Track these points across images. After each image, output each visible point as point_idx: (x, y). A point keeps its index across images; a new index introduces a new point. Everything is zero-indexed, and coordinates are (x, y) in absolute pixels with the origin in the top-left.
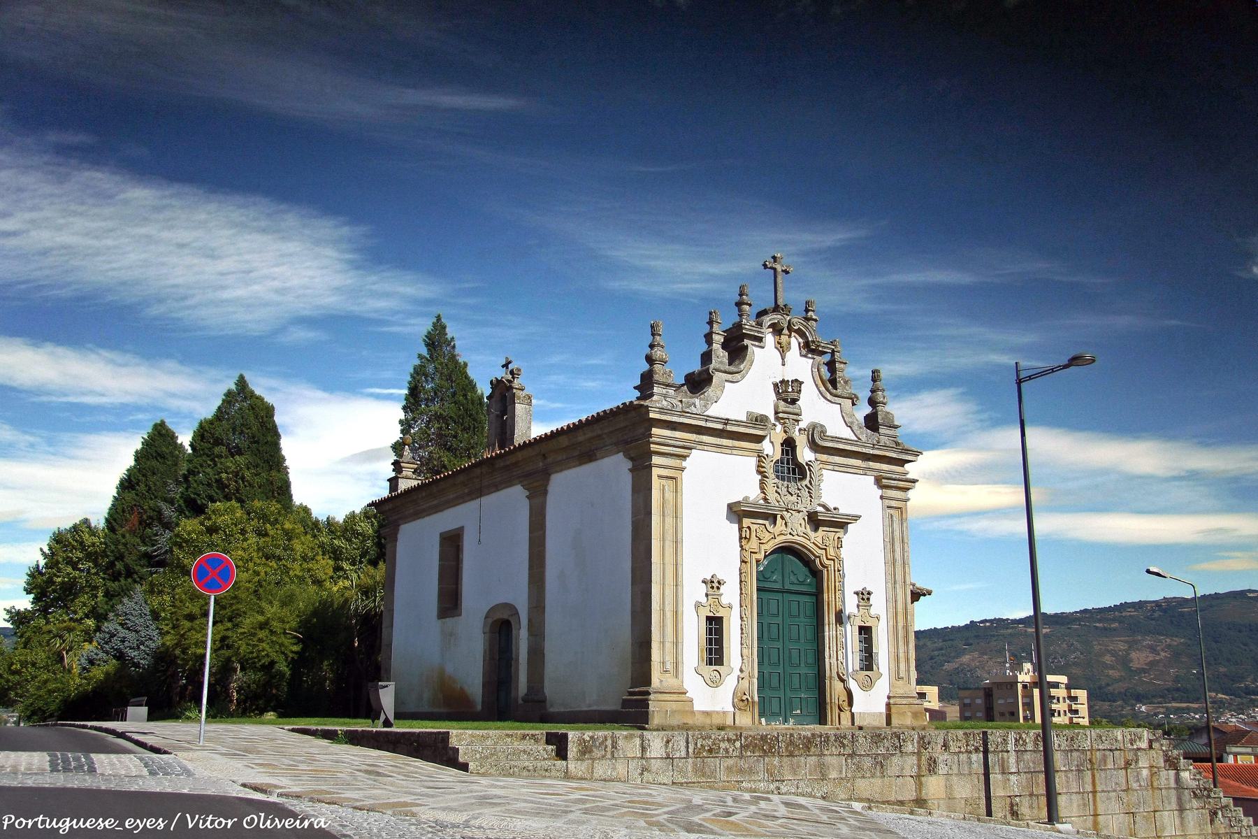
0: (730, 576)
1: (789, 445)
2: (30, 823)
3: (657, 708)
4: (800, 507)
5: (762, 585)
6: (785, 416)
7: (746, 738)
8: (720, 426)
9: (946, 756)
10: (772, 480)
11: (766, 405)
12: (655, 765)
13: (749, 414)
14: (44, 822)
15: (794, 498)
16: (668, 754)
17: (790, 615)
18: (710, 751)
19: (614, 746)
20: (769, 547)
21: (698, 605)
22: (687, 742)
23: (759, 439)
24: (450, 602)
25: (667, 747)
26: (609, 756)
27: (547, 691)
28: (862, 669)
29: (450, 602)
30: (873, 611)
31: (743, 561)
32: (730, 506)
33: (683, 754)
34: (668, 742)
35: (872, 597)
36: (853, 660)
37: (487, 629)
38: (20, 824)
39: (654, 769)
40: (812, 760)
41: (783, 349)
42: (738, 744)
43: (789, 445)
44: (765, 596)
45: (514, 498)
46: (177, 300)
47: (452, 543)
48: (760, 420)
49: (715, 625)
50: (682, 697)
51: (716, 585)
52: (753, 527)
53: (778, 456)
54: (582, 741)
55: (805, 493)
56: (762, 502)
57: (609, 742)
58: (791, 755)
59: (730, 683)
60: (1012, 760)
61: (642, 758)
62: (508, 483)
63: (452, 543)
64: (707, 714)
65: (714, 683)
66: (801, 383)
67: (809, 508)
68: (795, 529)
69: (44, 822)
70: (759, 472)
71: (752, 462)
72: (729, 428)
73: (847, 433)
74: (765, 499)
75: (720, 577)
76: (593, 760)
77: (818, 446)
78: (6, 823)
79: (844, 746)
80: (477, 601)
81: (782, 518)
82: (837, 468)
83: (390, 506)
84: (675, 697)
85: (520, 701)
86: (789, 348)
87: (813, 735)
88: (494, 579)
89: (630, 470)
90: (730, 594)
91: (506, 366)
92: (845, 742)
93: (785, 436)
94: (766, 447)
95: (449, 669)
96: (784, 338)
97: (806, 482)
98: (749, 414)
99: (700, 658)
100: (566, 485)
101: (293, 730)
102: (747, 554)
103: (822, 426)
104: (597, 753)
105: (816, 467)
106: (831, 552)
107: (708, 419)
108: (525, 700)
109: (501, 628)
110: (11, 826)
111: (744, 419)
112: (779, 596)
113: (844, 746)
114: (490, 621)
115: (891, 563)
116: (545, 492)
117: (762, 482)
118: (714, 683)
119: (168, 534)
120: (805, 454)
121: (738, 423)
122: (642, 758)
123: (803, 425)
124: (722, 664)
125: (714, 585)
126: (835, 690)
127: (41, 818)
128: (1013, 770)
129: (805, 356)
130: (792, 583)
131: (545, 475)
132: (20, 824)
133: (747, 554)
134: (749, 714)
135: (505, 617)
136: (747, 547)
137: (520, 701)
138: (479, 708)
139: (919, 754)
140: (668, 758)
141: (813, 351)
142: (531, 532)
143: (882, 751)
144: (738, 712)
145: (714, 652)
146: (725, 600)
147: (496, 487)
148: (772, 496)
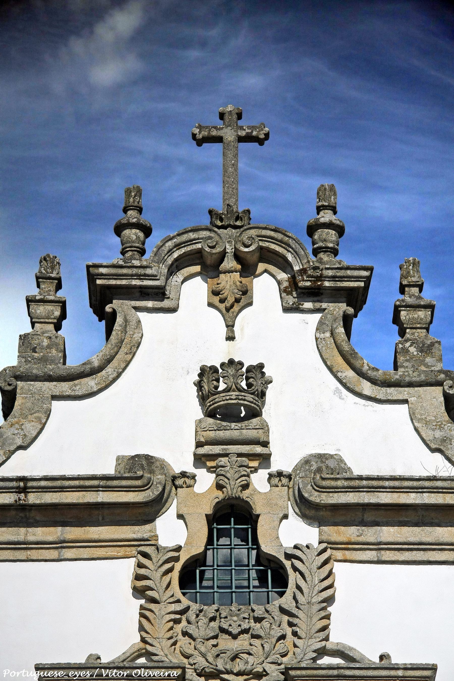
2: (18, 674)
14: (25, 673)
23: (148, 512)
38: (13, 674)
41: (231, 304)
46: (373, 382)
48: (140, 467)
66: (261, 366)
69: (25, 673)
70: (139, 592)
71: (124, 569)
72: (33, 498)
77: (317, 507)
78: (5, 674)
82: (382, 554)
97: (287, 601)
110: (8, 675)
111: (110, 470)
119: (263, 474)
121: (104, 482)
123: (284, 459)
127: (24, 671)
132: (13, 674)
141: (315, 293)
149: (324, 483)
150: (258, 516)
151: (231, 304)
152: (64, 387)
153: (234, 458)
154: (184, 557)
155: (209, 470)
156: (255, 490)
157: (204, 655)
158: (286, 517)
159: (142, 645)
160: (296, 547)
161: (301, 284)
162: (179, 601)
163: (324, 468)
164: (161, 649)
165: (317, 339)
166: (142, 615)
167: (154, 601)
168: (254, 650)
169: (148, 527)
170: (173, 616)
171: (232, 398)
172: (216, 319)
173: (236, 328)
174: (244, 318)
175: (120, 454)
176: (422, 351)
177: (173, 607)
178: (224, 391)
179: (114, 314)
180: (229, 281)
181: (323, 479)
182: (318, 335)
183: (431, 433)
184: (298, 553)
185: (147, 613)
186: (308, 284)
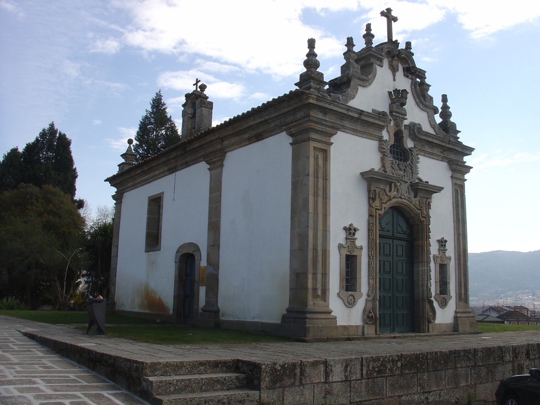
0: (361, 225)
3: (314, 324)
4: (406, 179)
5: (382, 233)
6: (397, 115)
7: (405, 358)
8: (356, 115)
9: (527, 362)
11: (383, 106)
12: (336, 388)
15: (402, 173)
16: (346, 377)
17: (397, 255)
18: (379, 372)
19: (302, 373)
20: (387, 206)
21: (340, 246)
22: (362, 365)
23: (381, 128)
24: (153, 240)
25: (346, 370)
26: (297, 383)
27: (220, 305)
29: (153, 240)
30: (447, 254)
32: (363, 174)
33: (358, 376)
34: (346, 366)
36: (434, 289)
37: (178, 260)
39: (335, 392)
40: (450, 372)
41: (394, 70)
42: (399, 364)
43: (398, 136)
45: (198, 173)
47: (156, 203)
49: (350, 262)
50: (328, 316)
51: (352, 231)
52: (378, 191)
53: (392, 142)
55: (408, 169)
56: (383, 172)
57: (298, 371)
58: (436, 370)
59: (361, 304)
61: (326, 382)
62: (196, 161)
63: (156, 203)
64: (345, 327)
65: (350, 304)
67: (412, 180)
68: (402, 195)
73: (432, 131)
74: (385, 171)
75: (355, 226)
76: (284, 387)
79: (469, 359)
80: (171, 242)
81: (395, 186)
84: (323, 316)
85: (200, 311)
88: (185, 224)
89: (291, 144)
90: (361, 239)
91: (196, 84)
92: (470, 356)
93: (397, 129)
95: (152, 285)
96: (395, 62)
99: (341, 287)
100: (240, 161)
101: (31, 337)
102: (373, 210)
103: (419, 124)
104: (288, 381)
105: (415, 152)
107: (350, 109)
108: (203, 310)
109: (187, 259)
112: (390, 241)
113: (469, 359)
114: (180, 254)
116: (222, 166)
118: (350, 304)
120: (409, 144)
122: (326, 382)
124: (355, 290)
125: (350, 231)
131: (222, 154)
133: (373, 210)
134: (374, 326)
135: (191, 252)
136: (374, 205)
137: (200, 311)
138: (171, 312)
139: (513, 361)
140: (346, 381)
142: (210, 193)
143: (491, 361)
144: (366, 326)
145: (350, 281)
146: (358, 243)
147: (187, 164)
148: (389, 170)
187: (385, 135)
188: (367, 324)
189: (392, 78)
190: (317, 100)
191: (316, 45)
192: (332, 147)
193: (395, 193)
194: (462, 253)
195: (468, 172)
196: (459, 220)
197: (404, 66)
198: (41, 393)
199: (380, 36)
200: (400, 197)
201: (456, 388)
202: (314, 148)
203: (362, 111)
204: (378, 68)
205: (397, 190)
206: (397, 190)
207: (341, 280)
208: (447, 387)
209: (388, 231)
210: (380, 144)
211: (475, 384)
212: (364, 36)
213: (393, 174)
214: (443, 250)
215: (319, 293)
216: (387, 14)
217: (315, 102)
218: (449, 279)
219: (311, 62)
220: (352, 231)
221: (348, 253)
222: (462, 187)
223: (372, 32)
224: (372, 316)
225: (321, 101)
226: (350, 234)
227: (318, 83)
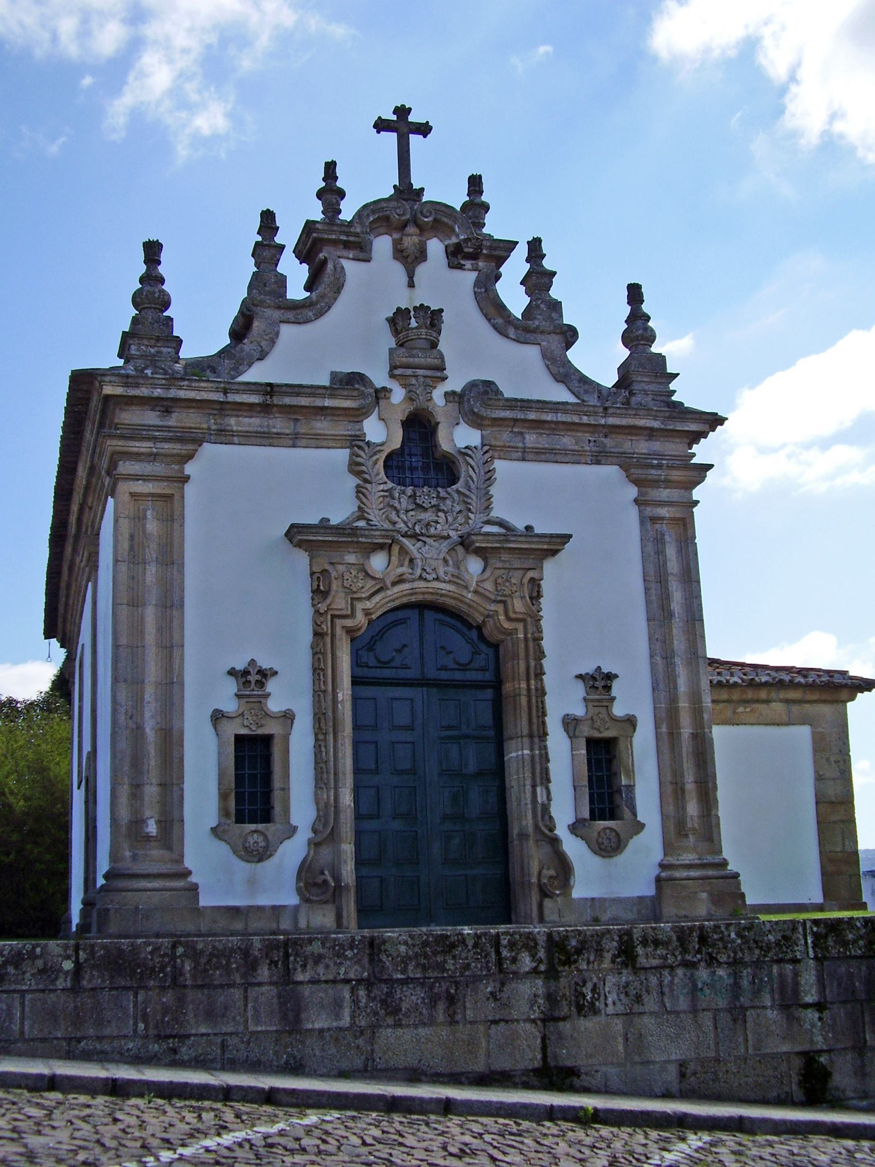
1: (419, 426)
5: (360, 672)
10: (381, 482)
13: (334, 375)
15: (428, 516)
23: (358, 415)
28: (593, 817)
31: (316, 634)
35: (616, 685)
36: (564, 805)
41: (410, 259)
44: (368, 691)
48: (351, 381)
54: (338, 1017)
60: (808, 978)
75: (264, 663)
83: (443, 208)
86: (422, 255)
87: (795, 961)
90: (290, 694)
94: (374, 430)
97: (460, 485)
98: (334, 375)
99: (224, 812)
106: (518, 605)
111: (327, 383)
115: (659, 614)
117: (359, 491)
118: (608, 848)
121: (313, 390)
123: (455, 383)
125: (252, 680)
126: (533, 861)
128: (809, 999)
129: (460, 267)
130: (445, 668)
149: (490, 402)
150: (439, 423)
151: (410, 259)
152: (290, 315)
153: (422, 379)
154: (387, 450)
155: (404, 386)
156: (435, 404)
157: (405, 523)
158: (458, 424)
159: (360, 513)
160: (467, 447)
161: (466, 250)
162: (386, 483)
163: (485, 390)
164: (376, 516)
165: (475, 293)
166: (358, 492)
167: (366, 481)
168: (440, 520)
169: (357, 427)
170: (382, 493)
171: (415, 331)
172: (398, 270)
173: (415, 279)
174: (421, 271)
175: (333, 370)
176: (549, 308)
177: (382, 487)
178: (416, 328)
179: (325, 262)
180: (410, 241)
181: (490, 399)
182: (476, 289)
183: (556, 369)
184: (470, 452)
185: (364, 491)
186: (471, 250)
187: (374, 430)
188: (308, 901)
189: (405, 280)
190: (126, 385)
191: (164, 256)
192: (189, 489)
193: (405, 569)
194: (684, 704)
195: (702, 479)
196: (669, 615)
197: (447, 243)
198: (42, 1101)
199: (368, 183)
200: (420, 577)
201: (290, 1033)
202: (132, 495)
203: (270, 385)
204: (351, 267)
205: (411, 561)
206: (411, 561)
207: (223, 796)
208: (252, 1028)
209: (483, 669)
210: (353, 454)
211: (374, 1028)
212: (320, 195)
213: (394, 523)
214: (259, 696)
215: (152, 828)
216: (402, 125)
217: (119, 391)
218: (630, 774)
219: (151, 298)
220: (253, 678)
221: (243, 731)
222: (685, 527)
223: (339, 184)
224: (325, 882)
225: (137, 386)
226: (247, 683)
227: (153, 342)
